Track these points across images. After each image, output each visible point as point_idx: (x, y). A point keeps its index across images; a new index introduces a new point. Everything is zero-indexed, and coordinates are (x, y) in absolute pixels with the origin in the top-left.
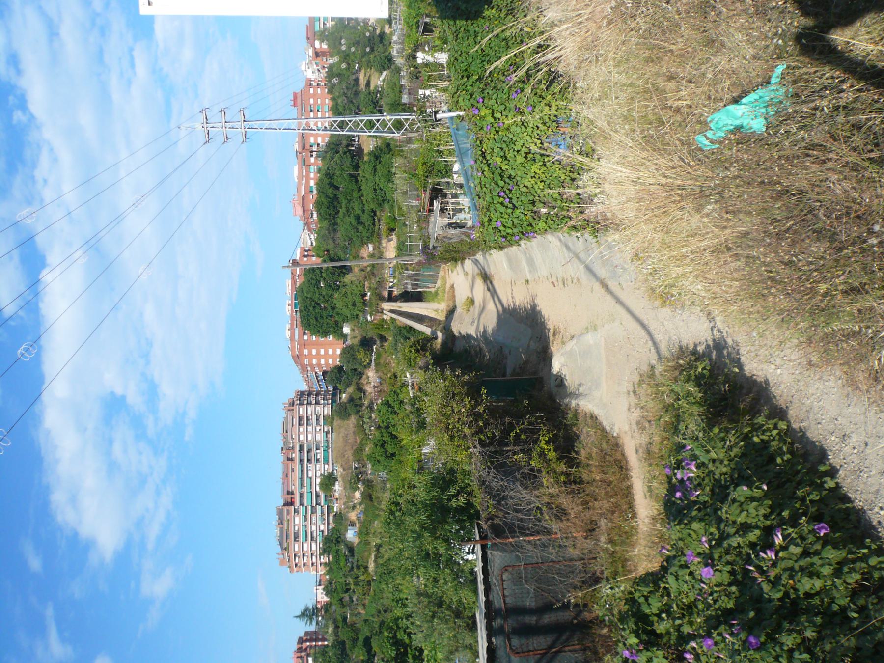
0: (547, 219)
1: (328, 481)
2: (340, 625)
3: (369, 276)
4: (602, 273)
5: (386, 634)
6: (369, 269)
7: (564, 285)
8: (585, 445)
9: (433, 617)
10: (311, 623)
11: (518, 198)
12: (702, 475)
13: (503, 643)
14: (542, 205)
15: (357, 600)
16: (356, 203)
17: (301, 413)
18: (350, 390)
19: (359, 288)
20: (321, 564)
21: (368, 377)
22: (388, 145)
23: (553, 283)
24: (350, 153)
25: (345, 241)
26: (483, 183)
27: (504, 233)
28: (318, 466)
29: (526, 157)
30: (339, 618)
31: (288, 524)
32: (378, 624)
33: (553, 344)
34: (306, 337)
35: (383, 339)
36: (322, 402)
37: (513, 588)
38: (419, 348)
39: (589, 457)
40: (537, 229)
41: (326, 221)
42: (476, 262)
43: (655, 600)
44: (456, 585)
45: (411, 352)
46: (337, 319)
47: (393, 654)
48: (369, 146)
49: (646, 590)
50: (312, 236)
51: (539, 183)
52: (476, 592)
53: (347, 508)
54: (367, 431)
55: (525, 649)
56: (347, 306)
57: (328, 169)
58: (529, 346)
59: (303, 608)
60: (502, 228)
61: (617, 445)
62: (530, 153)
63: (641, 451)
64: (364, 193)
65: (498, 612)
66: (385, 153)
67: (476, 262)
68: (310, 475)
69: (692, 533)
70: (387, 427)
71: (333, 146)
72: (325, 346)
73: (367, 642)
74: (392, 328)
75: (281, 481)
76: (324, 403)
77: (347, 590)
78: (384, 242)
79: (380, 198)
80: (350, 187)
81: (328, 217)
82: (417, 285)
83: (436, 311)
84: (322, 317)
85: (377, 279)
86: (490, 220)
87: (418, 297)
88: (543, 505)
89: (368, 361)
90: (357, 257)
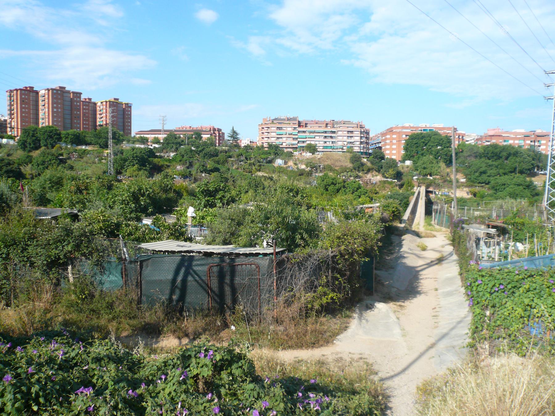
0: (482, 315)
1: (312, 149)
2: (227, 154)
3: (443, 179)
4: (442, 345)
5: (222, 185)
6: (448, 179)
7: (434, 316)
8: (330, 321)
9: (232, 220)
10: (229, 136)
11: (498, 296)
12: (312, 412)
13: (215, 261)
14: (492, 312)
15: (241, 164)
16: (495, 172)
17: (355, 132)
18: (369, 164)
19: (436, 172)
20: (263, 143)
21: (376, 176)
22: (537, 194)
23: (435, 308)
24: (532, 168)
25: (469, 163)
26: (510, 274)
27: (473, 284)
28: (322, 142)
29: (528, 305)
30: (231, 154)
31: (287, 124)
32: (227, 177)
33: (395, 304)
34: (404, 136)
35: (401, 186)
36: (362, 146)
37: (247, 271)
38: (395, 213)
39: (322, 324)
40: (475, 307)
41: (483, 151)
42: (451, 254)
43: (239, 372)
44: (249, 233)
45: (393, 208)
46: (415, 157)
47: (211, 189)
48: (537, 181)
49: (245, 367)
50: (473, 141)
51: (509, 312)
52: (245, 246)
53: (296, 160)
54: (342, 174)
55: (211, 275)
56: (423, 164)
57: (521, 153)
58: (393, 287)
59: (238, 132)
60: (477, 283)
61: (328, 342)
62: (531, 308)
63: (324, 358)
64: (502, 177)
65: (233, 260)
66: (531, 192)
67: (451, 254)
68: (316, 137)
69: (278, 402)
70: (344, 187)
71: (538, 156)
72: (398, 149)
73: (216, 170)
74: (408, 193)
75: (314, 120)
76: (361, 147)
77: (246, 159)
78: (466, 189)
79: (498, 188)
80: (507, 167)
81: (486, 152)
82: (436, 212)
83: (418, 224)
84: (417, 147)
85: (441, 184)
86: (483, 276)
87: (428, 212)
88: (294, 292)
89: (387, 176)
90: (457, 171)
